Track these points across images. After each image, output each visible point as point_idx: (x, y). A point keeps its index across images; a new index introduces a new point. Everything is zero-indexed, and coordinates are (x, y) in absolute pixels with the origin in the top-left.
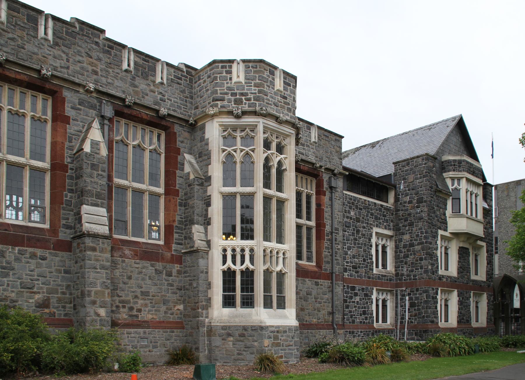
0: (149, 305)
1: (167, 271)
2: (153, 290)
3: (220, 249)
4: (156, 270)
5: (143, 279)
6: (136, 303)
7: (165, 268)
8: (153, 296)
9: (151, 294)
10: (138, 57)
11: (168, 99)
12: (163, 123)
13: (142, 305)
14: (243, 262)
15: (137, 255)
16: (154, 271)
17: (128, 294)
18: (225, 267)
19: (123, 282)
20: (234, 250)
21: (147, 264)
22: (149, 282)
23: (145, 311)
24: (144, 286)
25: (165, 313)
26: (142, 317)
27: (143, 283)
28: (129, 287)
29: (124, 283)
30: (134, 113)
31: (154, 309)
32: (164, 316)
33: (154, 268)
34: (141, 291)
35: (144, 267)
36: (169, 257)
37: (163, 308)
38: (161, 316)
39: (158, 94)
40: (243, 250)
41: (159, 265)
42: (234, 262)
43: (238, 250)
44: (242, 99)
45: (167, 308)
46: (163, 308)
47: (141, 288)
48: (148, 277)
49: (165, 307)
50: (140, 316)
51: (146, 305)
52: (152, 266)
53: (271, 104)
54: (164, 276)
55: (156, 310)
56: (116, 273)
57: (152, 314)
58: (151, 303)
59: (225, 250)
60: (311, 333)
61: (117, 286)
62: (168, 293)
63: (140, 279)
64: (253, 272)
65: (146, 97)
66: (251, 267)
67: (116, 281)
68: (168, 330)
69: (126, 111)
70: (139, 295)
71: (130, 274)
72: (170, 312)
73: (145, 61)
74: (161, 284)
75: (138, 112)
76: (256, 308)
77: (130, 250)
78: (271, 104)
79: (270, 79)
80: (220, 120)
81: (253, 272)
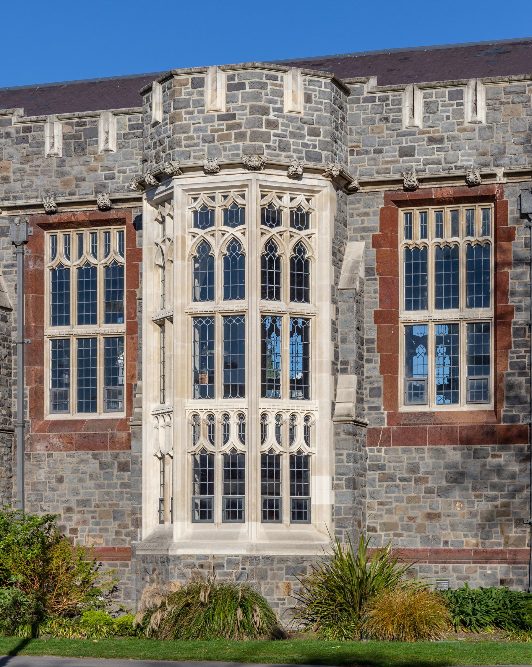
0: (91, 521)
1: (120, 464)
2: (96, 497)
3: (189, 416)
4: (100, 463)
5: (81, 480)
6: (69, 519)
7: (116, 457)
8: (97, 506)
9: (93, 504)
10: (67, 124)
11: (119, 172)
12: (112, 215)
13: (78, 523)
14: (226, 439)
15: (71, 443)
16: (98, 465)
17: (58, 507)
18: (197, 448)
19: (50, 488)
20: (211, 417)
21: (87, 455)
22: (90, 484)
23: (83, 531)
24: (81, 491)
25: (117, 533)
26: (78, 542)
27: (80, 488)
28: (60, 496)
29: (53, 489)
30: (65, 218)
31: (98, 527)
32: (114, 540)
33: (97, 461)
34: (77, 500)
35: (82, 461)
36: (124, 440)
37: (113, 526)
38: (111, 538)
39: (103, 170)
40: (226, 417)
41: (107, 455)
42: (212, 440)
43: (218, 417)
44: (269, 108)
45: (119, 525)
46: (113, 526)
47: (78, 494)
48: (88, 477)
49: (117, 523)
50: (75, 540)
51: (85, 522)
52: (95, 457)
53: (196, 145)
54: (115, 472)
55: (101, 530)
56: (40, 475)
57: (94, 537)
58: (93, 518)
59: (195, 416)
60: (454, 570)
61: (42, 494)
62: (122, 499)
63: (76, 481)
64: (243, 455)
65: (82, 184)
66: (240, 447)
67: (40, 487)
68: (118, 563)
69: (53, 219)
70: (73, 505)
71: (60, 473)
72: (124, 531)
73: (79, 125)
74: (109, 486)
75: (71, 214)
76: (246, 523)
77: (60, 437)
78: (196, 145)
79: (195, 97)
80: (184, 181)
81: (243, 455)
